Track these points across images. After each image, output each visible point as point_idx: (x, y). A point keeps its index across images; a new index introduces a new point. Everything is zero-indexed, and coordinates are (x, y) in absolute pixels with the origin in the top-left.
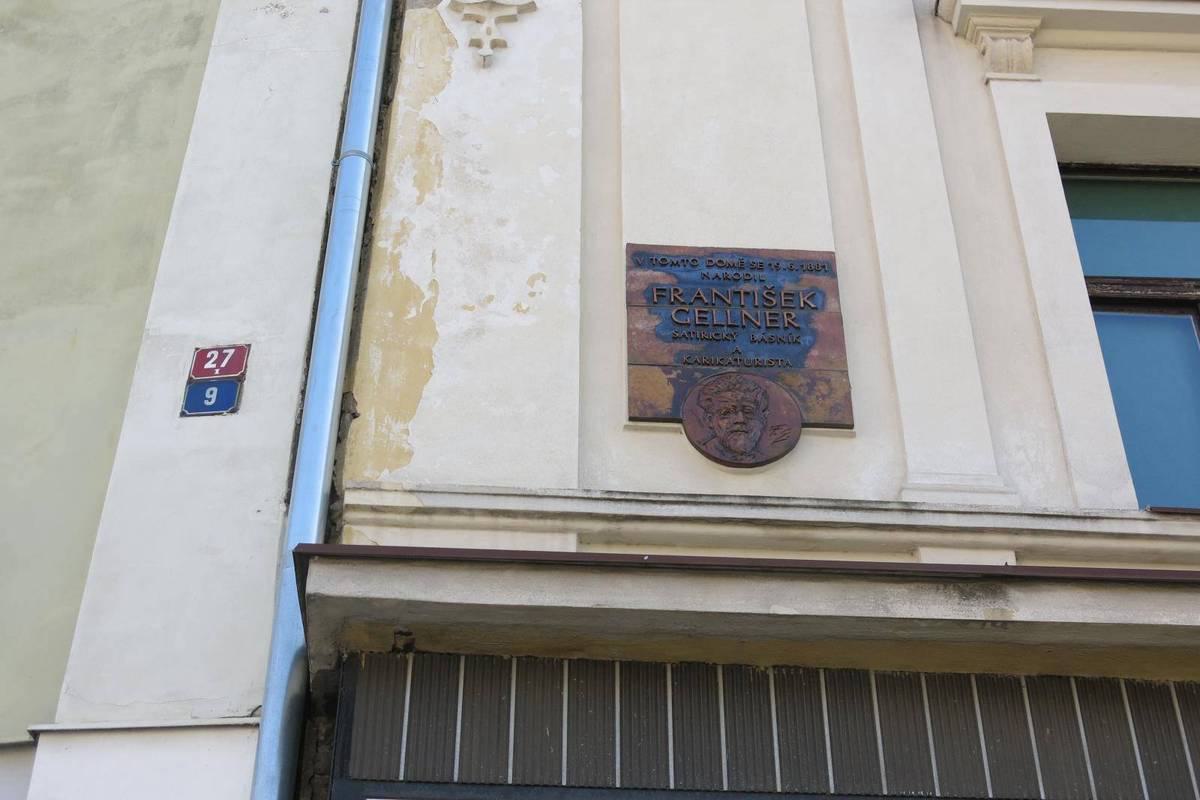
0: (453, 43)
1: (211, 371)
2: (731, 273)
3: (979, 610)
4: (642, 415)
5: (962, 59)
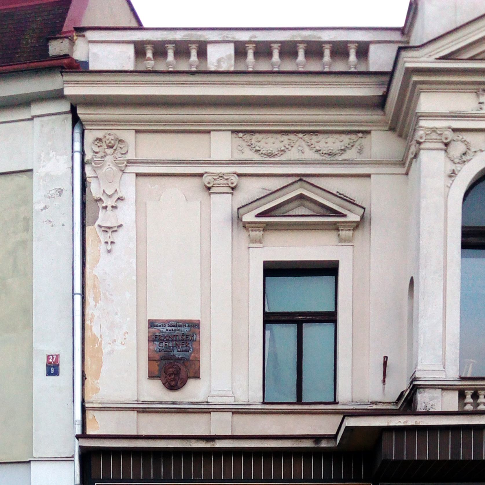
0: (100, 241)
1: (51, 363)
2: (173, 328)
3: (208, 445)
4: (151, 376)
5: (244, 234)
